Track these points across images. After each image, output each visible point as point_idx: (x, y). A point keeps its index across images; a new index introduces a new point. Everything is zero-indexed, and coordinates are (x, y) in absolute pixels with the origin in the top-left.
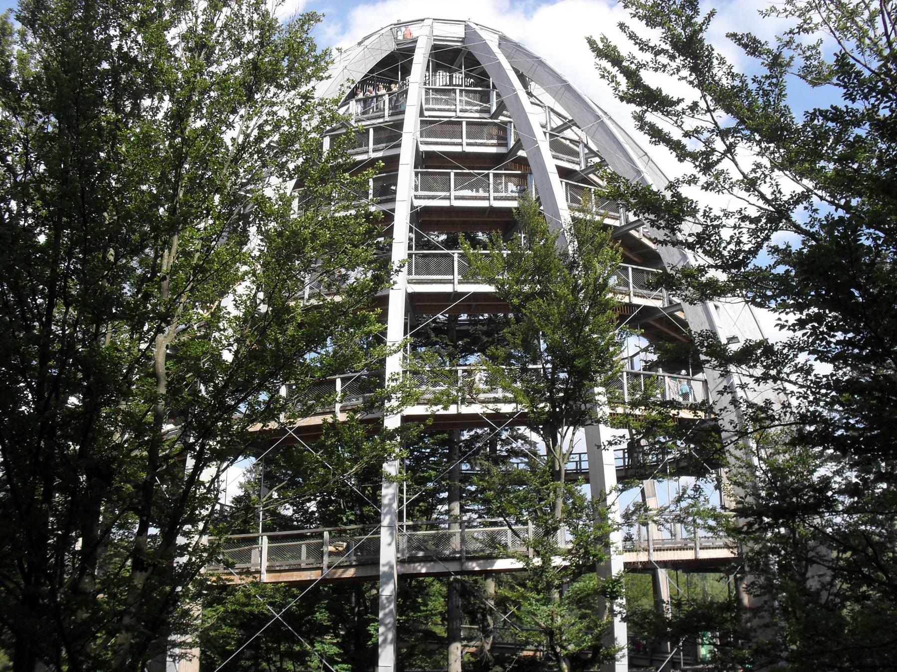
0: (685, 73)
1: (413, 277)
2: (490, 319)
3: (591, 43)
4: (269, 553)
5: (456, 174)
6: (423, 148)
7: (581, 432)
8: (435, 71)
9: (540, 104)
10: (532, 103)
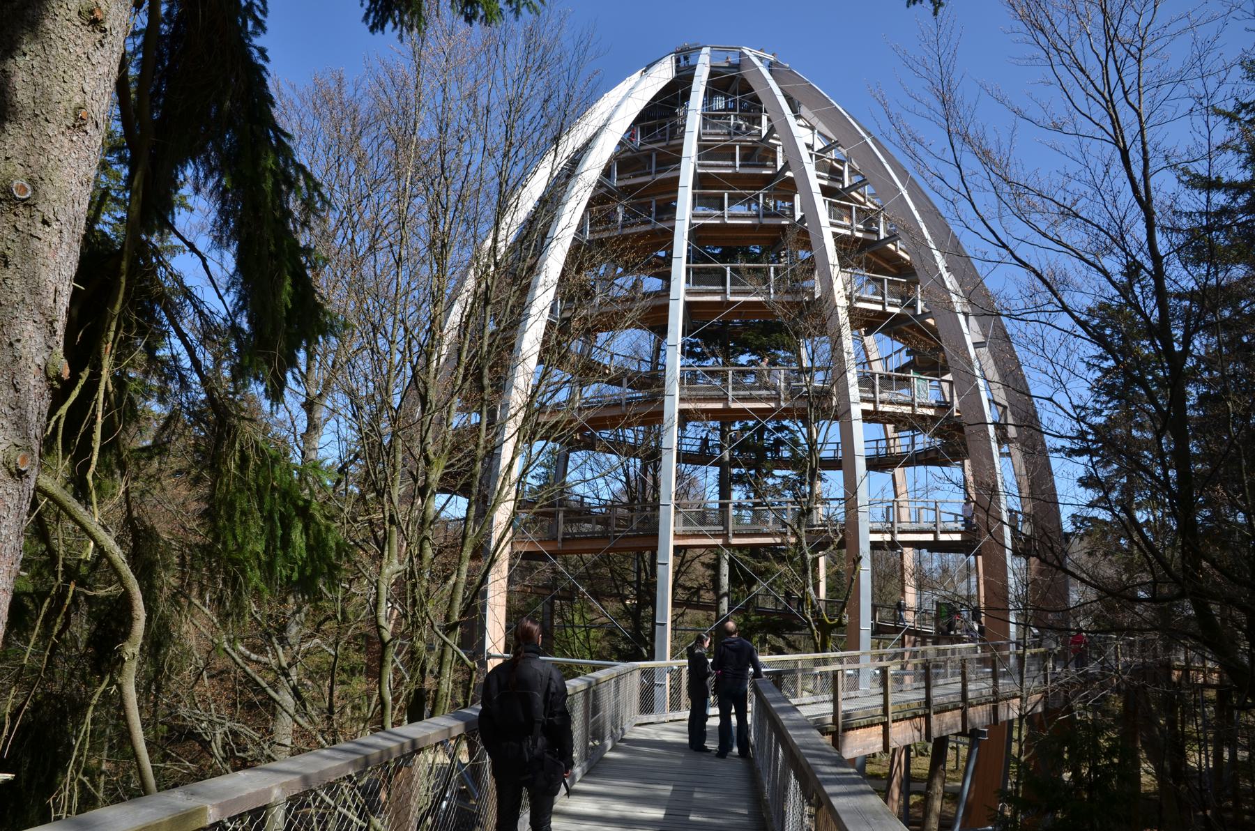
4: (693, 256)
7: (836, 426)
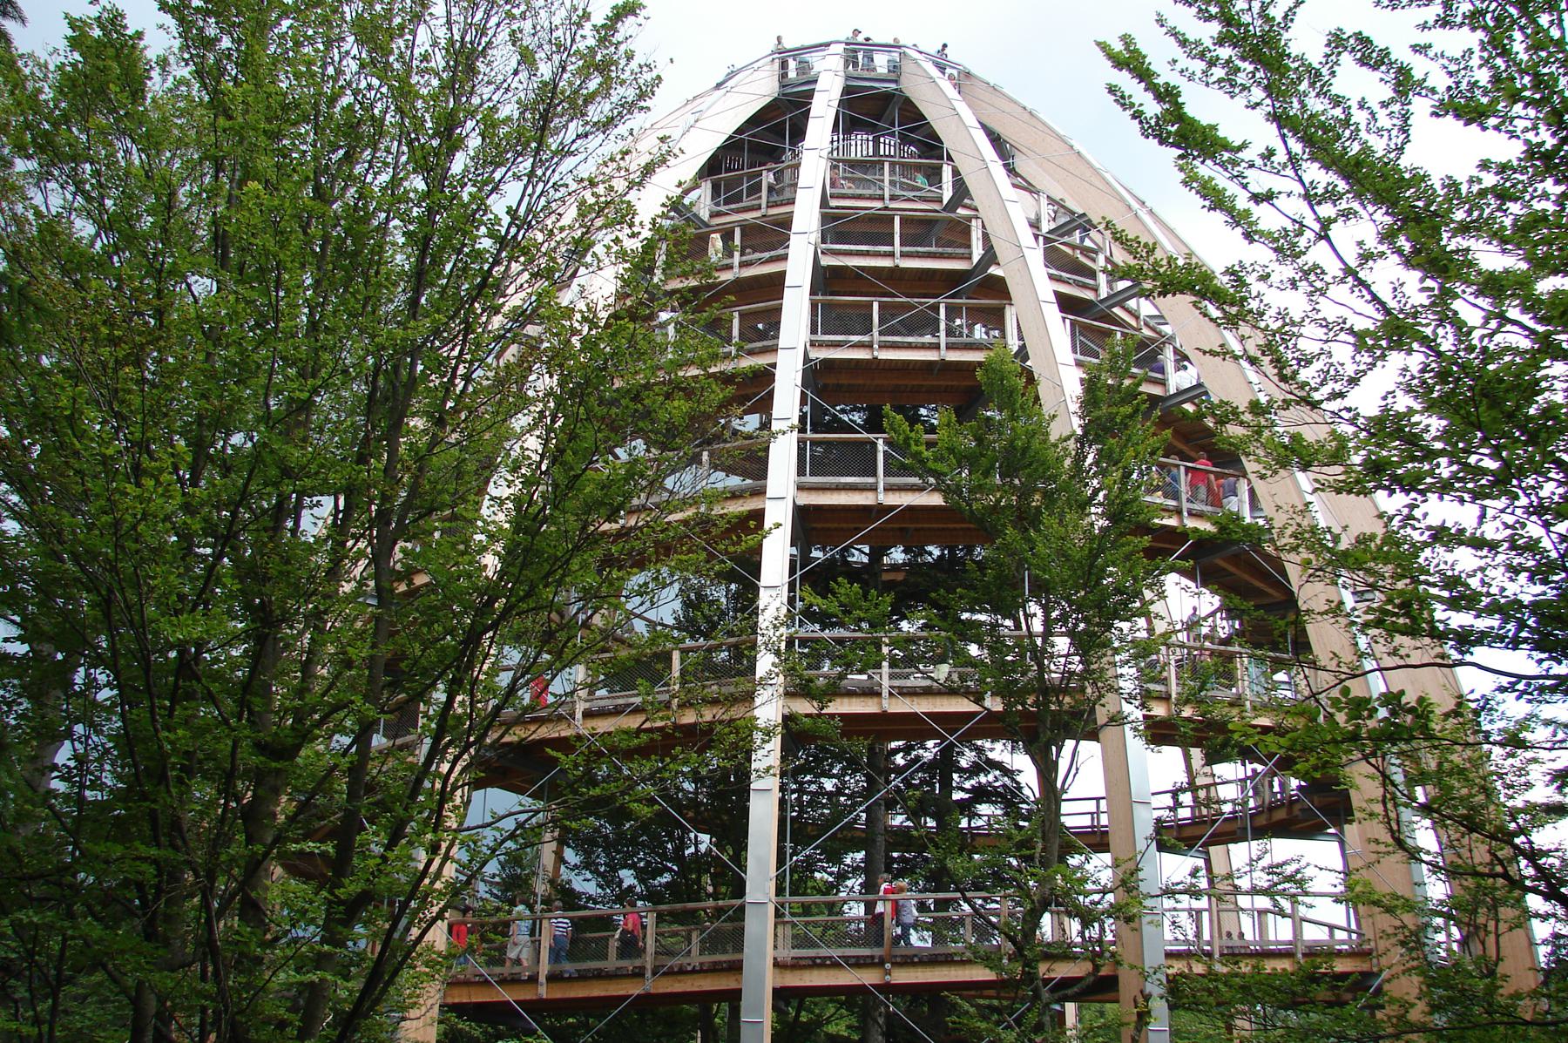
0: (1258, 94)
1: (809, 479)
3: (1104, 47)
4: (815, 419)
5: (882, 306)
6: (826, 261)
8: (848, 132)
9: (1030, 188)
10: (1015, 186)
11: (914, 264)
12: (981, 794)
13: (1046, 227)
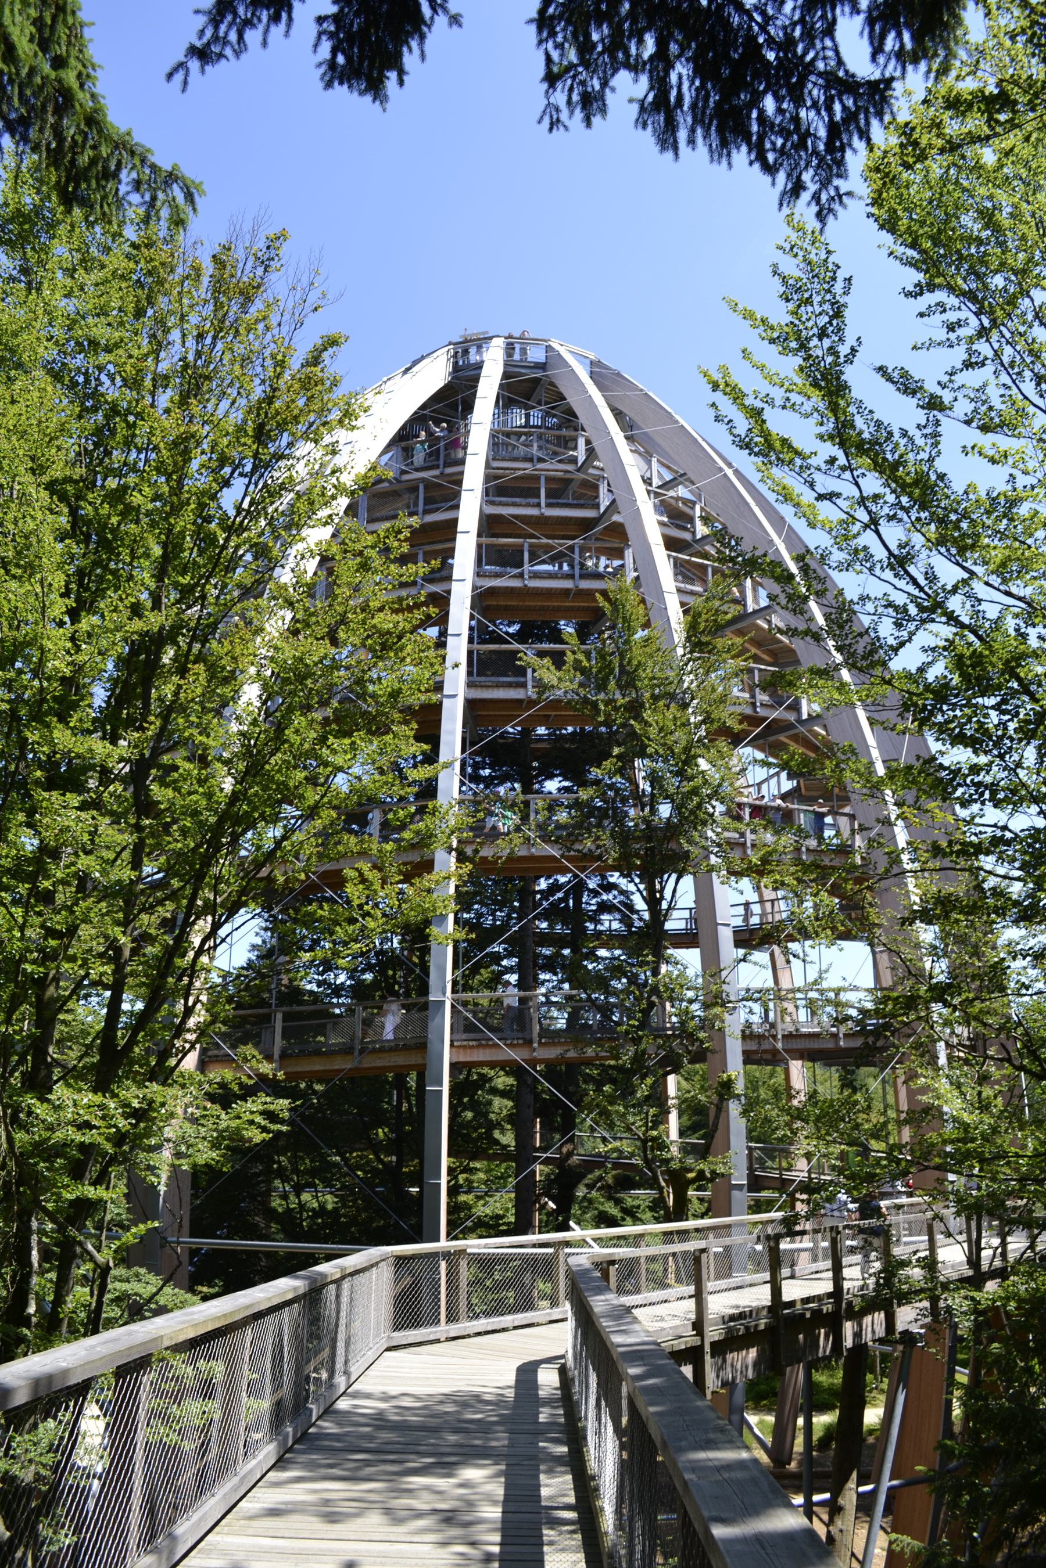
1: (475, 678)
2: (574, 732)
11: (555, 504)
12: (605, 907)
13: (656, 482)
